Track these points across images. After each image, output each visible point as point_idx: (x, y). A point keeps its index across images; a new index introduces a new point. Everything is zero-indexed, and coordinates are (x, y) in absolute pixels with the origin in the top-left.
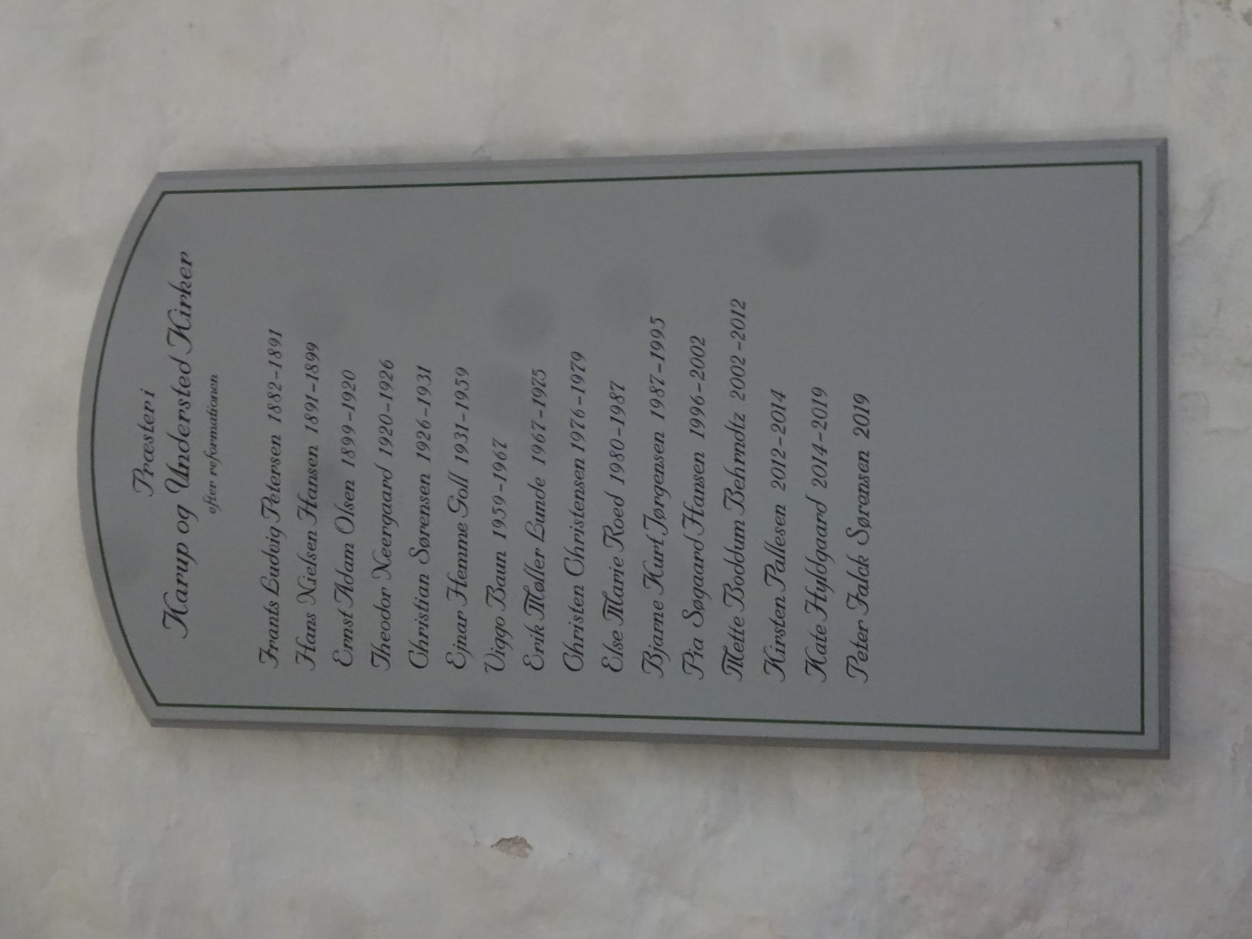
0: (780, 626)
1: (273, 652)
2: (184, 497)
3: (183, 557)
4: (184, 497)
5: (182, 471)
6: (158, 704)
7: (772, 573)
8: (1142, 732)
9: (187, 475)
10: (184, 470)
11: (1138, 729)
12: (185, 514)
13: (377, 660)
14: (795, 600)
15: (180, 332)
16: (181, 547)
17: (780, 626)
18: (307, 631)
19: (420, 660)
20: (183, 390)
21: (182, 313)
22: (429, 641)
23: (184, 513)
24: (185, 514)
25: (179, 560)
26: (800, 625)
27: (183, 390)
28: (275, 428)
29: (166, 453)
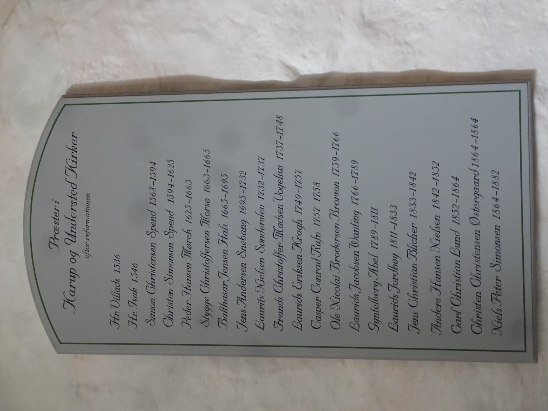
0: (170, 301)
1: (280, 322)
2: (74, 247)
3: (73, 275)
4: (74, 247)
5: (72, 236)
6: (61, 343)
7: (170, 277)
8: (525, 351)
9: (75, 236)
10: (74, 234)
11: (524, 350)
12: (74, 255)
13: (434, 329)
14: (177, 290)
15: (72, 169)
16: (72, 271)
17: (170, 301)
18: (278, 311)
19: (477, 330)
20: (73, 197)
21: (73, 161)
22: (482, 320)
23: (74, 254)
24: (74, 255)
25: (71, 276)
26: (180, 301)
27: (73, 197)
28: (436, 212)
29: (65, 226)
